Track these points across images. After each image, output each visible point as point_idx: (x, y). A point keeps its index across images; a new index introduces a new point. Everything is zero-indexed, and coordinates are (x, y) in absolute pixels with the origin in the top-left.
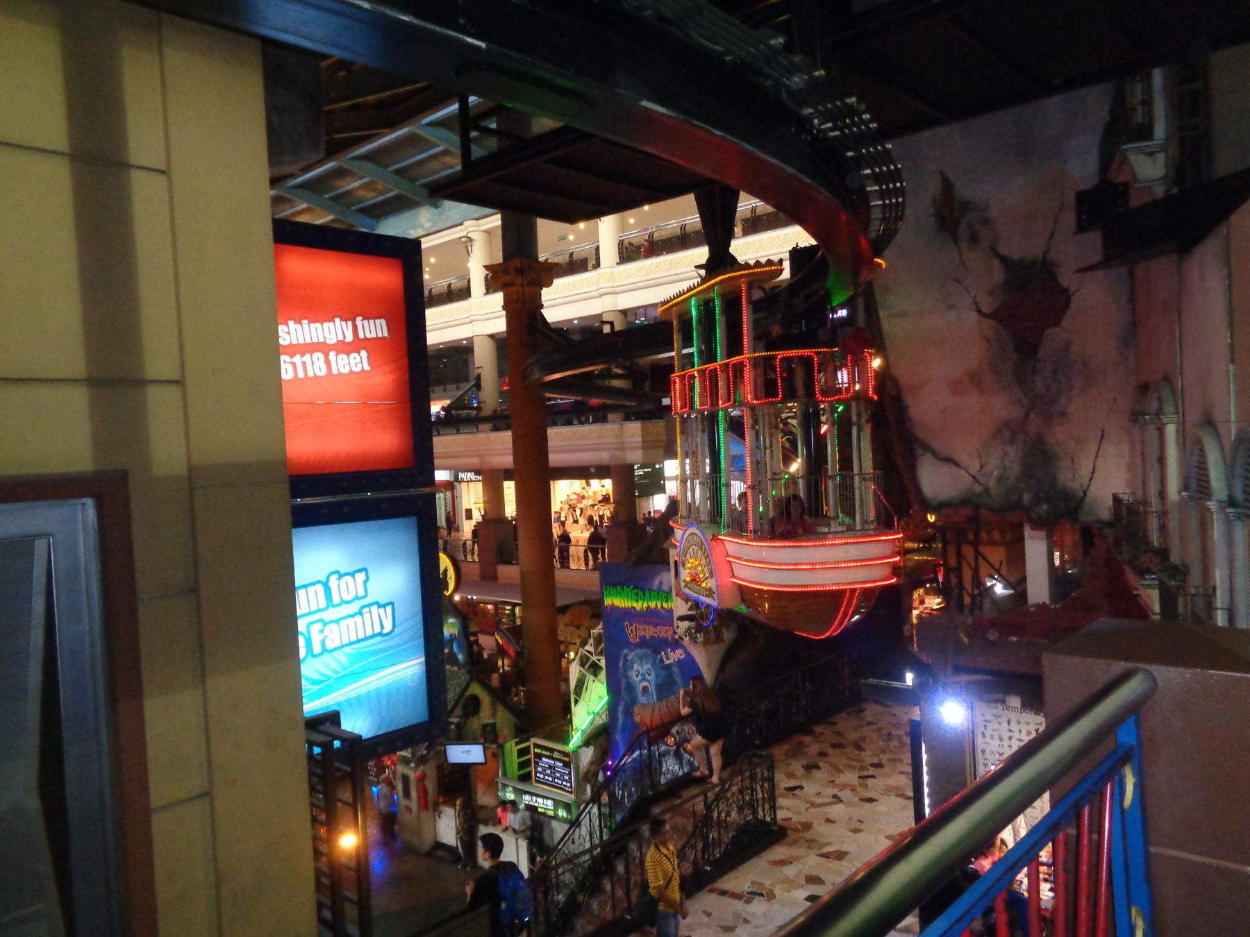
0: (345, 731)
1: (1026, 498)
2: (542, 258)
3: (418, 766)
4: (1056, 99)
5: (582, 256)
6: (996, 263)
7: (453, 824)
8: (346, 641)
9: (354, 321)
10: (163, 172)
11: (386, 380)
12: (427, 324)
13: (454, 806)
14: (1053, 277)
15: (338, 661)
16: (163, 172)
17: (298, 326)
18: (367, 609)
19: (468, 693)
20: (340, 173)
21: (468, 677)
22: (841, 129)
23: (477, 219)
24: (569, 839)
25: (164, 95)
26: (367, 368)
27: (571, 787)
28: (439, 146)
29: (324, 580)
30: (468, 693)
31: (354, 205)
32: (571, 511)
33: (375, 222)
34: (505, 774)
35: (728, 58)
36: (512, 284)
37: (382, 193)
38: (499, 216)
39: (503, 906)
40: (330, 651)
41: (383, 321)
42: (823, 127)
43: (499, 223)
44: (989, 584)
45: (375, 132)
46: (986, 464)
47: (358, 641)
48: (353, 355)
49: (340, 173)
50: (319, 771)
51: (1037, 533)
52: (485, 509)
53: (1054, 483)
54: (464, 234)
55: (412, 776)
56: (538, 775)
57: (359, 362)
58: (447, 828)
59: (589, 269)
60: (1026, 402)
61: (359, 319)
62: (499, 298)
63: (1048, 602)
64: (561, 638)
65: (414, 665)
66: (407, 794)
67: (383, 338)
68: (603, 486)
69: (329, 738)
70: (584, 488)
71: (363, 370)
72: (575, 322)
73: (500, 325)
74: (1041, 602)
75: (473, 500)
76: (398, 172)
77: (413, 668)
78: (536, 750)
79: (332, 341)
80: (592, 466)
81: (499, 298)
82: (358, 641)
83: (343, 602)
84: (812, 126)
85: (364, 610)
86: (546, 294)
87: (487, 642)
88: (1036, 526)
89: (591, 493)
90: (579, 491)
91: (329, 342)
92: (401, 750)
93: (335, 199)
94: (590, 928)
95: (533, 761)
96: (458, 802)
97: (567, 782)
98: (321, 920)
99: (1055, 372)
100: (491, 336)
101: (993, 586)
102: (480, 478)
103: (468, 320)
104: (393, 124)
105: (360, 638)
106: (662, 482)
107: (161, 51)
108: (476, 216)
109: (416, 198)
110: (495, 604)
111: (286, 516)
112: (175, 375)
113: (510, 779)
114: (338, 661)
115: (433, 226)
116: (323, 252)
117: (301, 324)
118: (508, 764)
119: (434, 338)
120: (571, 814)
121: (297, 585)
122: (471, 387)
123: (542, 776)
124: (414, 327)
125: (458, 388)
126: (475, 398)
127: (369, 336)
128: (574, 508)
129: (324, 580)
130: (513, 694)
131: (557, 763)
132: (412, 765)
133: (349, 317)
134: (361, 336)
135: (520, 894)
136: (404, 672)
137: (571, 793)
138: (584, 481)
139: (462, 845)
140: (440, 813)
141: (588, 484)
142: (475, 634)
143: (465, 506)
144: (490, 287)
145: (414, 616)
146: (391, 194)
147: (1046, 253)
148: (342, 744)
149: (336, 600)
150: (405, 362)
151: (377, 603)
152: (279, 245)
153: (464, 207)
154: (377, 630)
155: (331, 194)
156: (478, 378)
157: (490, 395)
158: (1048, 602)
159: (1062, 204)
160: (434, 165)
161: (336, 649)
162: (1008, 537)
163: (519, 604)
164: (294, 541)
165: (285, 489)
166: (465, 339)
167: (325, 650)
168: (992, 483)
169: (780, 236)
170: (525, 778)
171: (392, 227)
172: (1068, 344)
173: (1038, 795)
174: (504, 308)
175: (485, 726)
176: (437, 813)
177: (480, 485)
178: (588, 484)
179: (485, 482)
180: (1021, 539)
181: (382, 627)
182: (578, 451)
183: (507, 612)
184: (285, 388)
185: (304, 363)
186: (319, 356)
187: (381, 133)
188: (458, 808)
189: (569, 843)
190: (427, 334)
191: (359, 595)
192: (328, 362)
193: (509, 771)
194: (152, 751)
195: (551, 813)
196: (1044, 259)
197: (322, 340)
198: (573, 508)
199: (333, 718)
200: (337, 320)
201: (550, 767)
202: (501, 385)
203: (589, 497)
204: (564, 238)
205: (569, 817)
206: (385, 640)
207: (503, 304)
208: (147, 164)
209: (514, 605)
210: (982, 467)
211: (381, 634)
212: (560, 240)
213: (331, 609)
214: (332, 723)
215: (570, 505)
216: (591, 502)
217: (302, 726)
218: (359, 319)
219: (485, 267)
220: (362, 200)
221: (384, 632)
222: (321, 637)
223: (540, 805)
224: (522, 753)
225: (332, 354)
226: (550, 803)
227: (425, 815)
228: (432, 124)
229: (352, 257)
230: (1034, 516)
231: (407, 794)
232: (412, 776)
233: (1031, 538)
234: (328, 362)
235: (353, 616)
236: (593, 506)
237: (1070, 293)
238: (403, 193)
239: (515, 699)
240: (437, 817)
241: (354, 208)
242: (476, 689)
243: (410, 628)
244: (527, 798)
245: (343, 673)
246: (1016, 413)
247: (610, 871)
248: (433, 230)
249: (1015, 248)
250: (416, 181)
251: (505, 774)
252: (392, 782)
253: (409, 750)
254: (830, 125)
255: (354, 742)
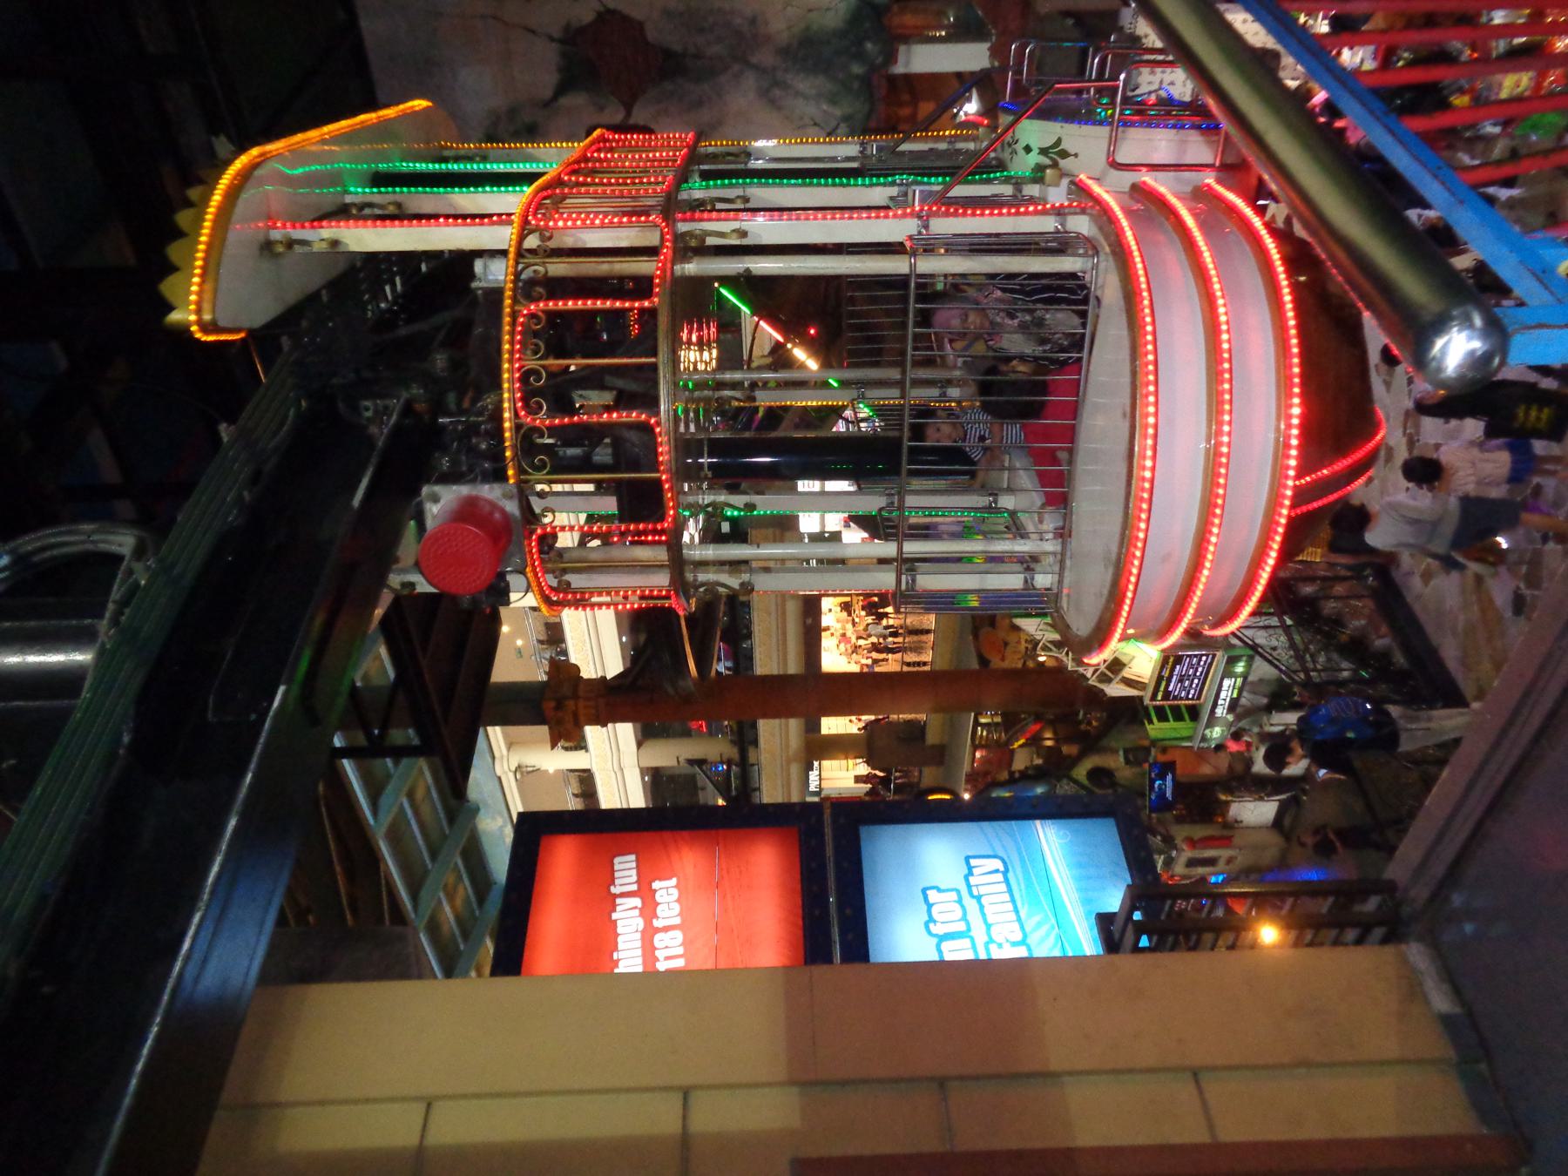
0: (1121, 907)
1: (857, 69)
2: (545, 678)
3: (1175, 847)
4: (364, 24)
5: (542, 628)
6: (564, 101)
7: (1251, 805)
8: (1013, 916)
9: (616, 896)
10: (429, 1105)
11: (690, 859)
12: (619, 806)
13: (1227, 803)
14: (582, 30)
15: (1039, 925)
16: (429, 1105)
17: (621, 964)
18: (974, 889)
19: (1086, 782)
20: (434, 928)
21: (1065, 781)
22: (394, 275)
23: (493, 758)
24: (1271, 655)
25: (333, 1102)
26: (674, 881)
27: (1207, 656)
28: (402, 804)
29: (935, 940)
30: (1086, 782)
31: (473, 912)
32: (860, 651)
33: (494, 886)
34: (1189, 738)
35: (304, 404)
36: (575, 715)
37: (460, 878)
38: (490, 729)
39: (1350, 735)
40: (1025, 936)
41: (617, 860)
42: (390, 297)
43: (498, 729)
44: (963, 118)
45: (383, 882)
46: (812, 119)
47: (1013, 901)
48: (658, 897)
49: (434, 928)
50: (1171, 939)
51: (901, 58)
52: (856, 758)
53: (841, 34)
54: (511, 775)
55: (1188, 853)
56: (1190, 696)
57: (666, 891)
58: (1256, 812)
59: (557, 620)
60: (736, 67)
61: (614, 890)
62: (592, 732)
63: (988, 45)
64: (1020, 665)
65: (1045, 834)
66: (1211, 862)
67: (637, 860)
68: (830, 610)
69: (1130, 927)
70: (832, 634)
71: (676, 887)
72: (624, 639)
73: (625, 731)
74: (988, 53)
75: (844, 774)
76: (434, 855)
77: (1049, 834)
78: (1159, 697)
79: (640, 923)
80: (805, 622)
81: (592, 732)
82: (1013, 901)
83: (964, 918)
84: (389, 310)
85: (975, 892)
86: (588, 672)
87: (1022, 760)
88: (891, 57)
89: (839, 626)
90: (834, 641)
91: (641, 927)
92: (1156, 867)
93: (466, 934)
94: (1384, 629)
95: (1172, 702)
96: (1223, 798)
97: (1200, 660)
98: (1359, 941)
99: (701, 31)
100: (639, 744)
101: (966, 114)
102: (816, 764)
103: (619, 774)
104: (374, 859)
105: (1009, 899)
106: (826, 535)
107: (278, 1105)
108: (490, 760)
109: (466, 835)
110: (975, 748)
111: (858, 967)
112: (676, 1100)
113: (1195, 733)
114: (1039, 925)
115: (502, 816)
116: (530, 931)
117: (618, 960)
118: (1174, 735)
119: (637, 799)
120: (1242, 656)
121: (936, 958)
122: (703, 771)
123: (1192, 692)
124: (623, 824)
125: (703, 789)
126: (717, 768)
127: (634, 878)
128: (856, 647)
129: (935, 940)
130: (1089, 728)
131: (1176, 673)
132: (1174, 853)
133: (611, 901)
134: (634, 887)
135: (1334, 714)
136: (1053, 848)
137: (1214, 656)
138: (823, 634)
139: (1277, 795)
140: (1236, 821)
141: (827, 629)
142: (1012, 773)
143: (850, 783)
144: (580, 744)
145: (986, 835)
146: (460, 862)
147: (552, 39)
148: (1137, 909)
149: (961, 927)
150: (667, 835)
151: (966, 878)
152: (523, 969)
153: (475, 774)
154: (1000, 877)
155: (460, 940)
156: (691, 762)
157: (716, 749)
158: (988, 45)
159: (495, 18)
160: (425, 809)
161: (1022, 927)
162: (906, 97)
163: (976, 720)
164: (887, 960)
165: (819, 971)
166: (643, 779)
167: (1023, 942)
168: (838, 112)
169: (526, 376)
170: (1194, 713)
171: (499, 862)
172: (667, 13)
173: (1228, 28)
174: (604, 725)
175: (1127, 761)
176: (1236, 825)
177: (825, 763)
178: (827, 629)
179: (820, 758)
180: (910, 79)
181: (997, 871)
182: (784, 634)
183: (985, 733)
184: (693, 967)
185: (668, 958)
186: (659, 940)
187: (385, 877)
188: (1230, 798)
189: (1275, 654)
190: (632, 806)
191: (956, 898)
192: (666, 929)
193: (1185, 733)
194: (1141, 1140)
195: (1239, 681)
196: (561, 41)
197: (638, 936)
198: (856, 649)
199: (1105, 921)
200: (614, 916)
201: (1181, 681)
202: (700, 734)
203: (844, 628)
204: (519, 651)
205: (1244, 658)
206: (1013, 867)
207: (599, 727)
208: (420, 1121)
209: (977, 723)
210: (815, 124)
211: (1005, 873)
212: (521, 656)
213: (972, 934)
214: (1112, 924)
215: (853, 652)
216: (849, 626)
217: (1114, 957)
218: (614, 890)
219: (553, 748)
220: (467, 900)
221: (1002, 869)
222: (1007, 946)
223: (1229, 694)
224: (1162, 716)
225: (657, 923)
226: (1227, 683)
227: (1237, 841)
228: (375, 813)
229: (537, 888)
230: (880, 60)
231: (1211, 862)
232: (1188, 853)
233: (907, 63)
234: (666, 929)
235: (982, 907)
236: (854, 624)
237: (602, 9)
238: (460, 847)
239: (1094, 723)
240: (1241, 825)
241: (477, 913)
242: (1081, 772)
243: (1001, 841)
244: (1219, 711)
245: (1053, 921)
246: (750, 81)
247: (1312, 602)
248: (506, 815)
249: (547, 80)
250: (444, 834)
251: (1189, 738)
252: (1197, 881)
253: (1156, 857)
254: (388, 288)
255: (1135, 898)
